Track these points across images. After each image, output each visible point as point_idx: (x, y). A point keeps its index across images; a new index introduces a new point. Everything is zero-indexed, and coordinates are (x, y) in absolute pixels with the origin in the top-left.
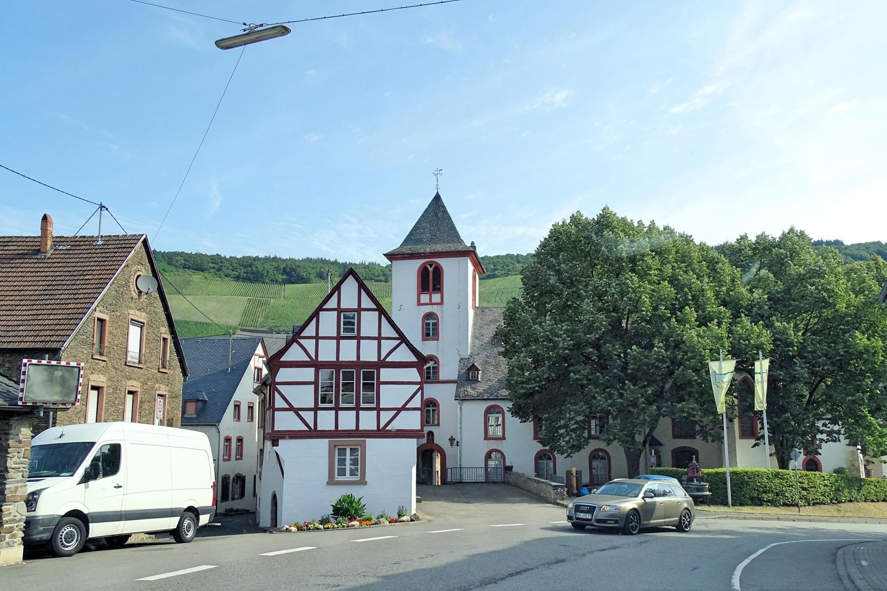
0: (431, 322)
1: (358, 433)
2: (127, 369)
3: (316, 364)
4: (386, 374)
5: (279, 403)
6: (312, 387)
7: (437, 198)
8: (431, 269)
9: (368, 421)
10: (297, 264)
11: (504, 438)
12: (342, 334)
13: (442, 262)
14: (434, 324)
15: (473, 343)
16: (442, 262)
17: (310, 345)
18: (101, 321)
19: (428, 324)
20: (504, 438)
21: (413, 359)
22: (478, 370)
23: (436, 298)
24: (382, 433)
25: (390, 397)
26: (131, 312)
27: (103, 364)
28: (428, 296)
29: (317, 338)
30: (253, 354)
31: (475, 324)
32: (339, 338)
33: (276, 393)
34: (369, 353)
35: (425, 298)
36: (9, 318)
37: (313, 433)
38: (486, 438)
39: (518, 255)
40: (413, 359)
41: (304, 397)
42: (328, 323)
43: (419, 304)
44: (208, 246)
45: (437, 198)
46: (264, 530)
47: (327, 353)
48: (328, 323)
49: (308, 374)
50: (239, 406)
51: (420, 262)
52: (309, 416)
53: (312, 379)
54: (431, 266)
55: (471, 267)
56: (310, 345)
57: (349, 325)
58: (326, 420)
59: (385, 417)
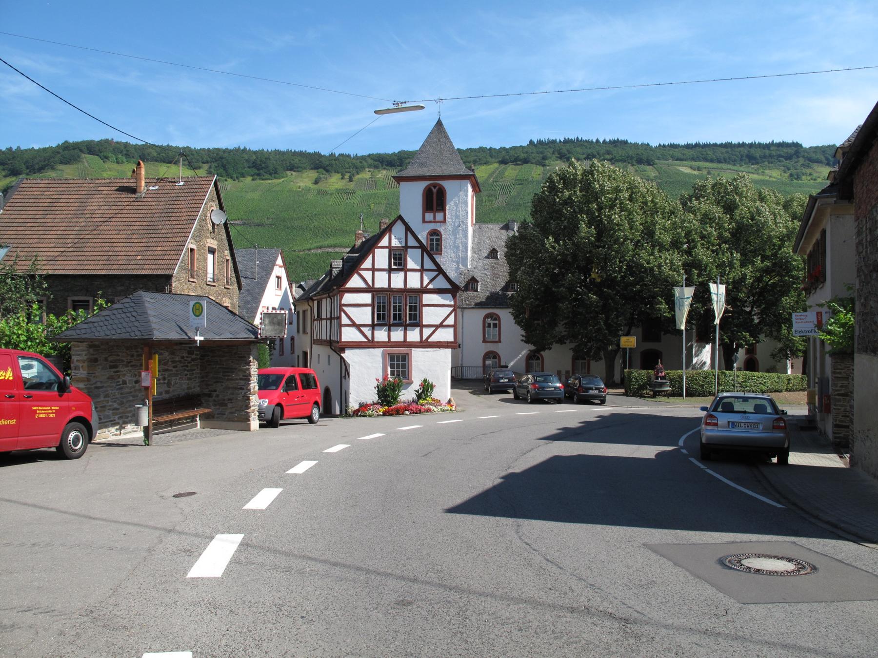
0: (435, 238)
1: (405, 344)
2: (207, 287)
3: (369, 289)
4: (427, 298)
5: (345, 320)
6: (370, 308)
7: (439, 123)
8: (435, 191)
9: (413, 335)
10: (266, 156)
11: (500, 341)
12: (393, 267)
13: (446, 184)
14: (438, 240)
15: (472, 257)
16: (446, 184)
17: (368, 275)
18: (192, 250)
19: (432, 240)
20: (500, 341)
21: (448, 286)
22: (478, 282)
23: (439, 216)
24: (424, 344)
25: (430, 316)
26: (208, 240)
27: (194, 284)
28: (432, 215)
29: (373, 270)
30: (274, 264)
31: (474, 237)
32: (390, 270)
33: (343, 314)
34: (414, 281)
35: (429, 216)
36: (127, 249)
37: (371, 344)
38: (484, 341)
39: (491, 149)
40: (448, 286)
41: (364, 316)
42: (381, 257)
43: (424, 221)
44: (179, 142)
45: (439, 123)
46: (337, 416)
47: (381, 281)
48: (381, 257)
49: (367, 298)
50: (733, 423)
51: (424, 184)
52: (367, 331)
53: (369, 302)
54: (435, 187)
55: (470, 189)
56: (368, 275)
57: (398, 261)
58: (381, 335)
59: (427, 332)
